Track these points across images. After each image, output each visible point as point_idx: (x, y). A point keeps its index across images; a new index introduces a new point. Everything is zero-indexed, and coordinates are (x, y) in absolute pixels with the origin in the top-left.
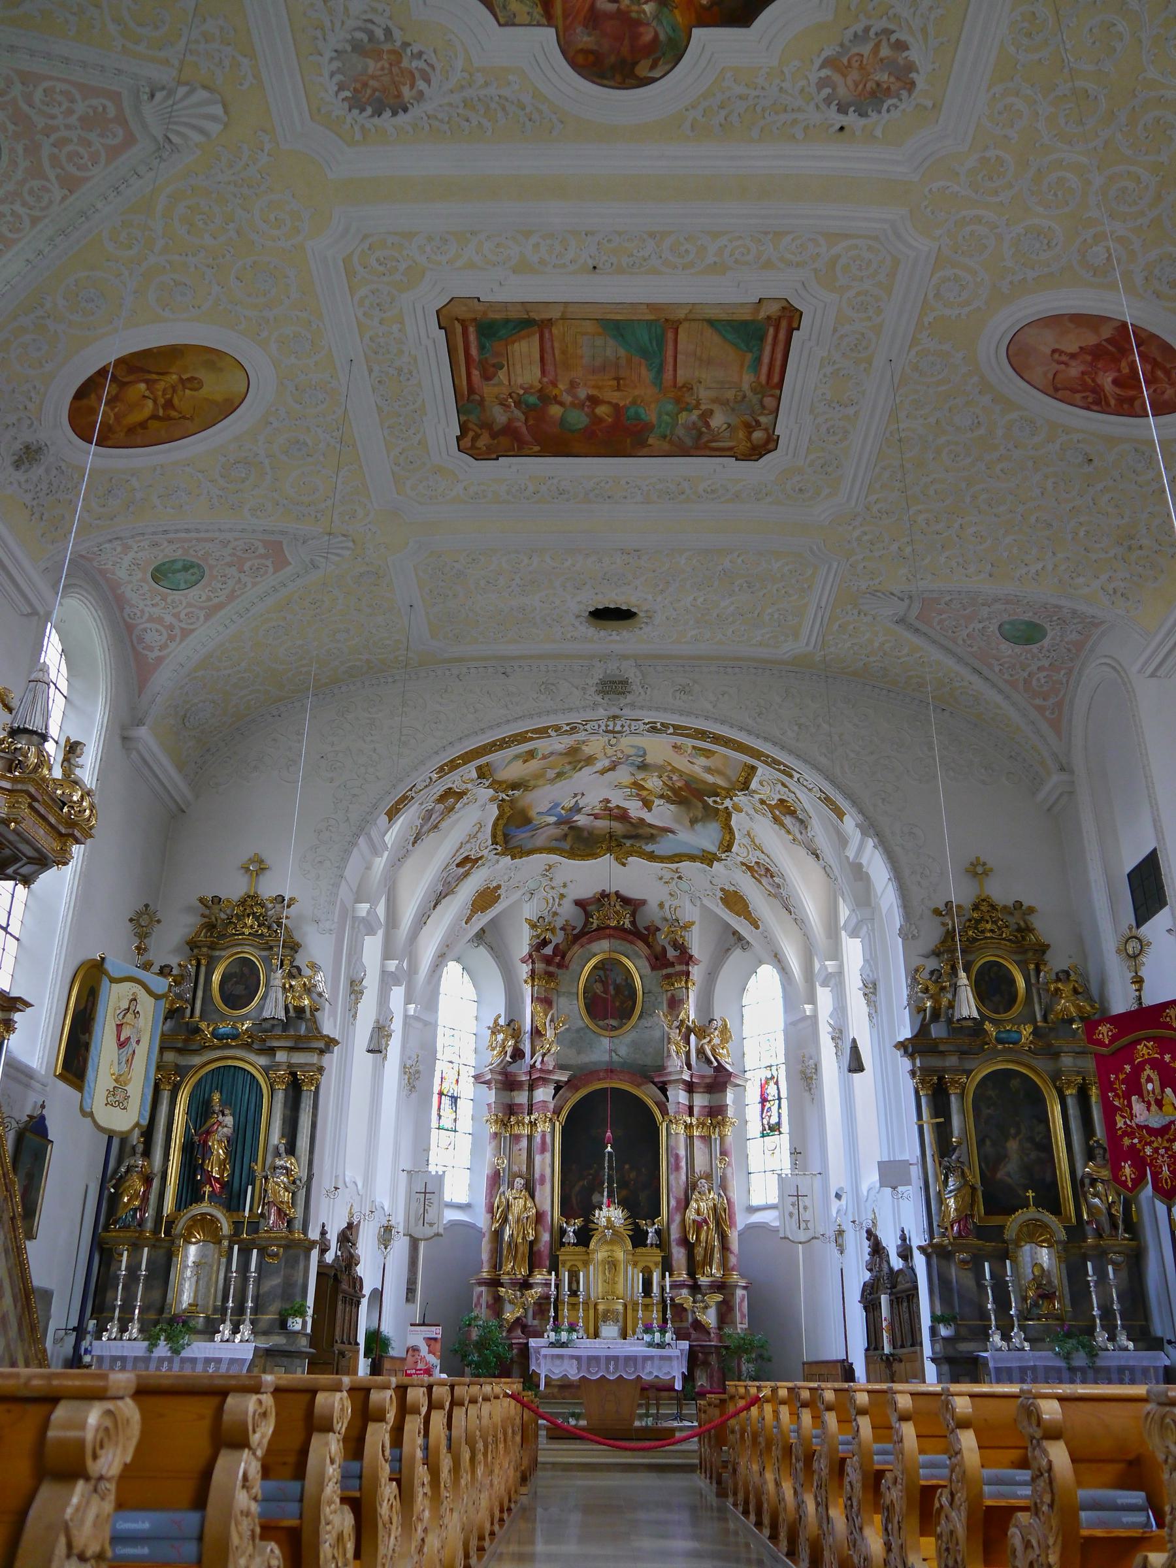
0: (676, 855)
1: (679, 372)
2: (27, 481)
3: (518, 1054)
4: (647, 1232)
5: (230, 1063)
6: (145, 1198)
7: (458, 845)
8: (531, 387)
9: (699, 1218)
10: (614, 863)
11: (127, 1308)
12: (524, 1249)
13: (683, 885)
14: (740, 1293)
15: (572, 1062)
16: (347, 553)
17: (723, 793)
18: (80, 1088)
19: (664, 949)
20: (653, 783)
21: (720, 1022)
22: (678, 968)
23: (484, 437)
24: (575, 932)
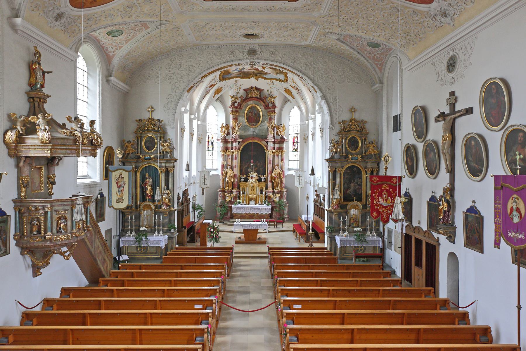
3: (228, 134)
14: (285, 193)
22: (272, 109)
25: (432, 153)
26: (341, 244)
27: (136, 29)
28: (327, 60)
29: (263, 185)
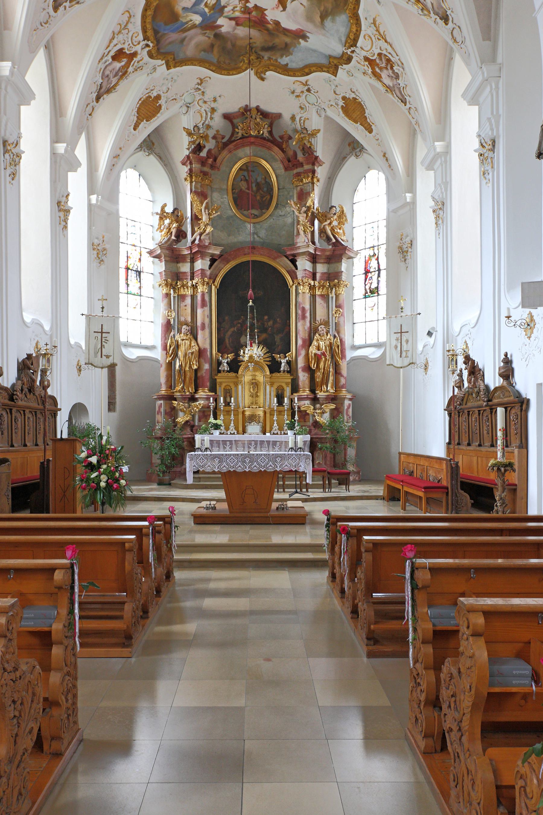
0: (306, 66)
3: (181, 235)
4: (281, 363)
7: (110, 35)
9: (319, 353)
10: (254, 78)
12: (190, 375)
13: (312, 98)
14: (347, 402)
19: (295, 154)
22: (307, 167)
24: (225, 140)
29: (284, 379)
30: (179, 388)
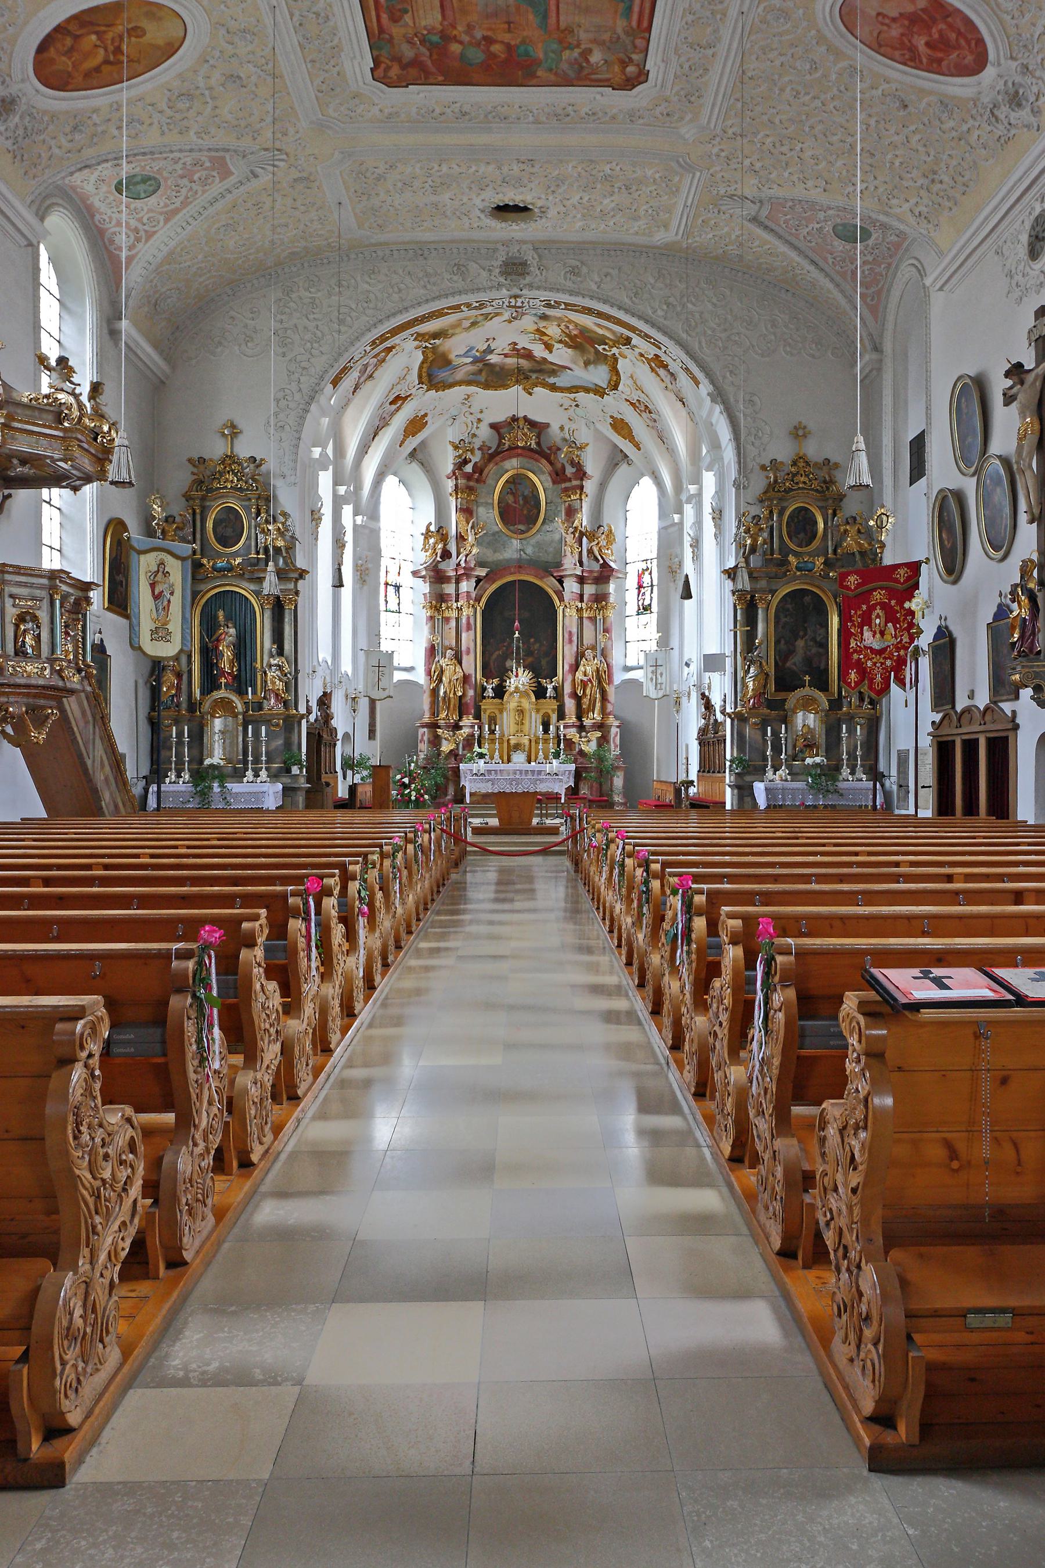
1: (562, 18)
2: (6, 130)
3: (446, 555)
5: (228, 588)
6: (179, 688)
8: (434, 28)
9: (585, 679)
11: (180, 762)
14: (614, 730)
15: (490, 559)
16: (281, 164)
17: (611, 343)
18: (127, 617)
19: (563, 468)
20: (553, 331)
21: (606, 528)
22: (575, 483)
23: (393, 67)
25: (998, 490)
26: (768, 799)
27: (196, 177)
28: (728, 292)
29: (550, 706)
30: (443, 715)
